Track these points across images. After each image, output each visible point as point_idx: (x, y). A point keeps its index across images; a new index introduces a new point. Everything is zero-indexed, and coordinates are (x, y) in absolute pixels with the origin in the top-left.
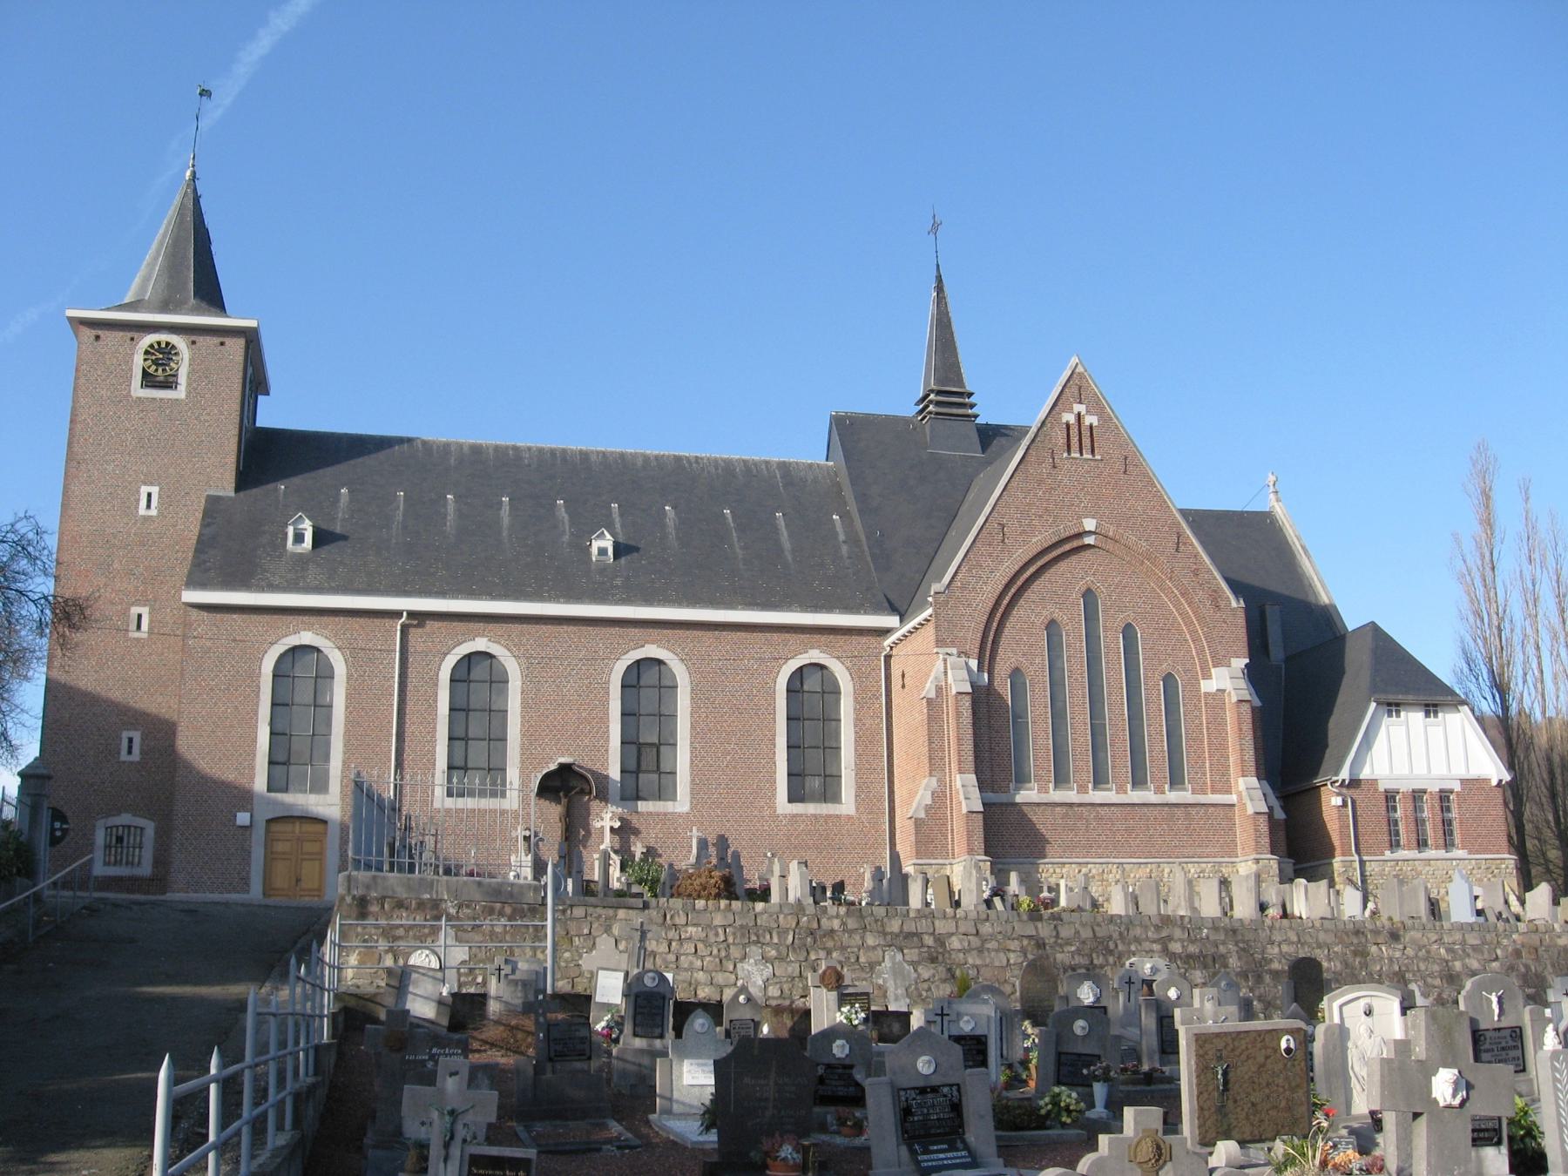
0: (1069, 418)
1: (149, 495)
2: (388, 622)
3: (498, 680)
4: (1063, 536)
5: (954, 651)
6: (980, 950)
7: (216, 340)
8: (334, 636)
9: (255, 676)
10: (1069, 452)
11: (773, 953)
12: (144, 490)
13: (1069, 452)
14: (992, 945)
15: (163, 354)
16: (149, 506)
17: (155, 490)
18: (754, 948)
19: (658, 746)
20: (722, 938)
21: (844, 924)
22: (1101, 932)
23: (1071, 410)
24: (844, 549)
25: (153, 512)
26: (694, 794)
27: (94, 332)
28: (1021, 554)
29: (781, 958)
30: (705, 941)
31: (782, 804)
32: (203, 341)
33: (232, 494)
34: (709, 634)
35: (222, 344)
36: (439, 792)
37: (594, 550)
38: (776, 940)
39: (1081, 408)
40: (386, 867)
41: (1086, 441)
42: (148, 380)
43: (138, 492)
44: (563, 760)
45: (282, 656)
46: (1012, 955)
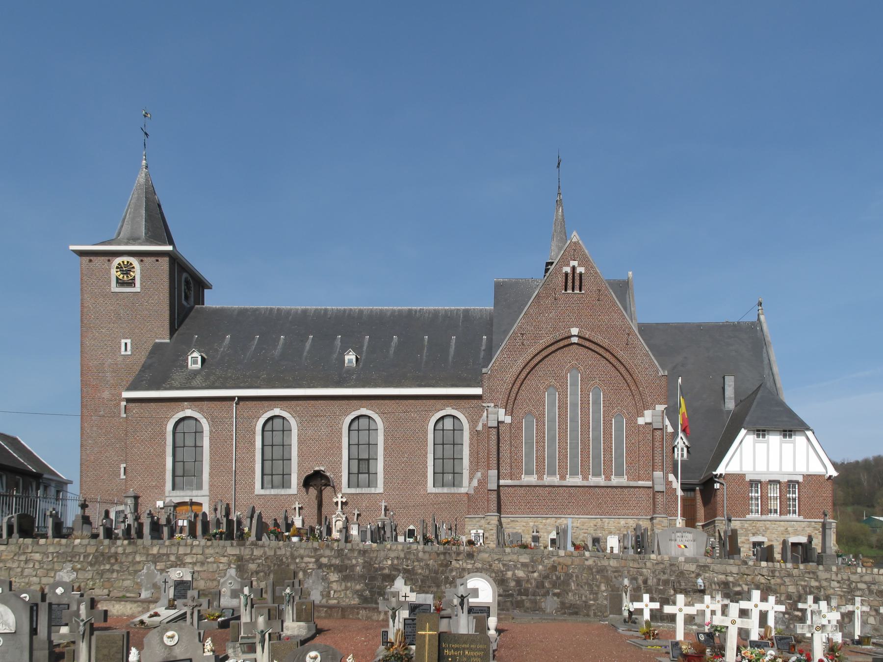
0: (568, 269)
1: (126, 344)
2: (229, 403)
3: (286, 430)
4: (558, 339)
5: (493, 405)
6: (202, 564)
7: (154, 259)
8: (201, 411)
9: (163, 434)
10: (566, 290)
11: (79, 566)
12: (123, 341)
13: (566, 290)
14: (211, 560)
15: (126, 269)
16: (126, 350)
17: (129, 341)
18: (68, 564)
19: (368, 460)
20: (50, 559)
21: (124, 550)
22: (279, 553)
23: (568, 265)
24: (482, 353)
25: (129, 353)
26: (385, 483)
27: (88, 258)
28: (533, 351)
29: (83, 569)
30: (40, 562)
31: (258, 490)
32: (148, 260)
33: (168, 341)
34: (393, 401)
35: (90, 261)
36: (258, 484)
37: (346, 361)
38: (82, 559)
39: (575, 263)
40: (775, 505)
41: (577, 283)
42: (120, 283)
43: (120, 343)
44: (317, 469)
45: (353, 421)
46: (221, 565)
